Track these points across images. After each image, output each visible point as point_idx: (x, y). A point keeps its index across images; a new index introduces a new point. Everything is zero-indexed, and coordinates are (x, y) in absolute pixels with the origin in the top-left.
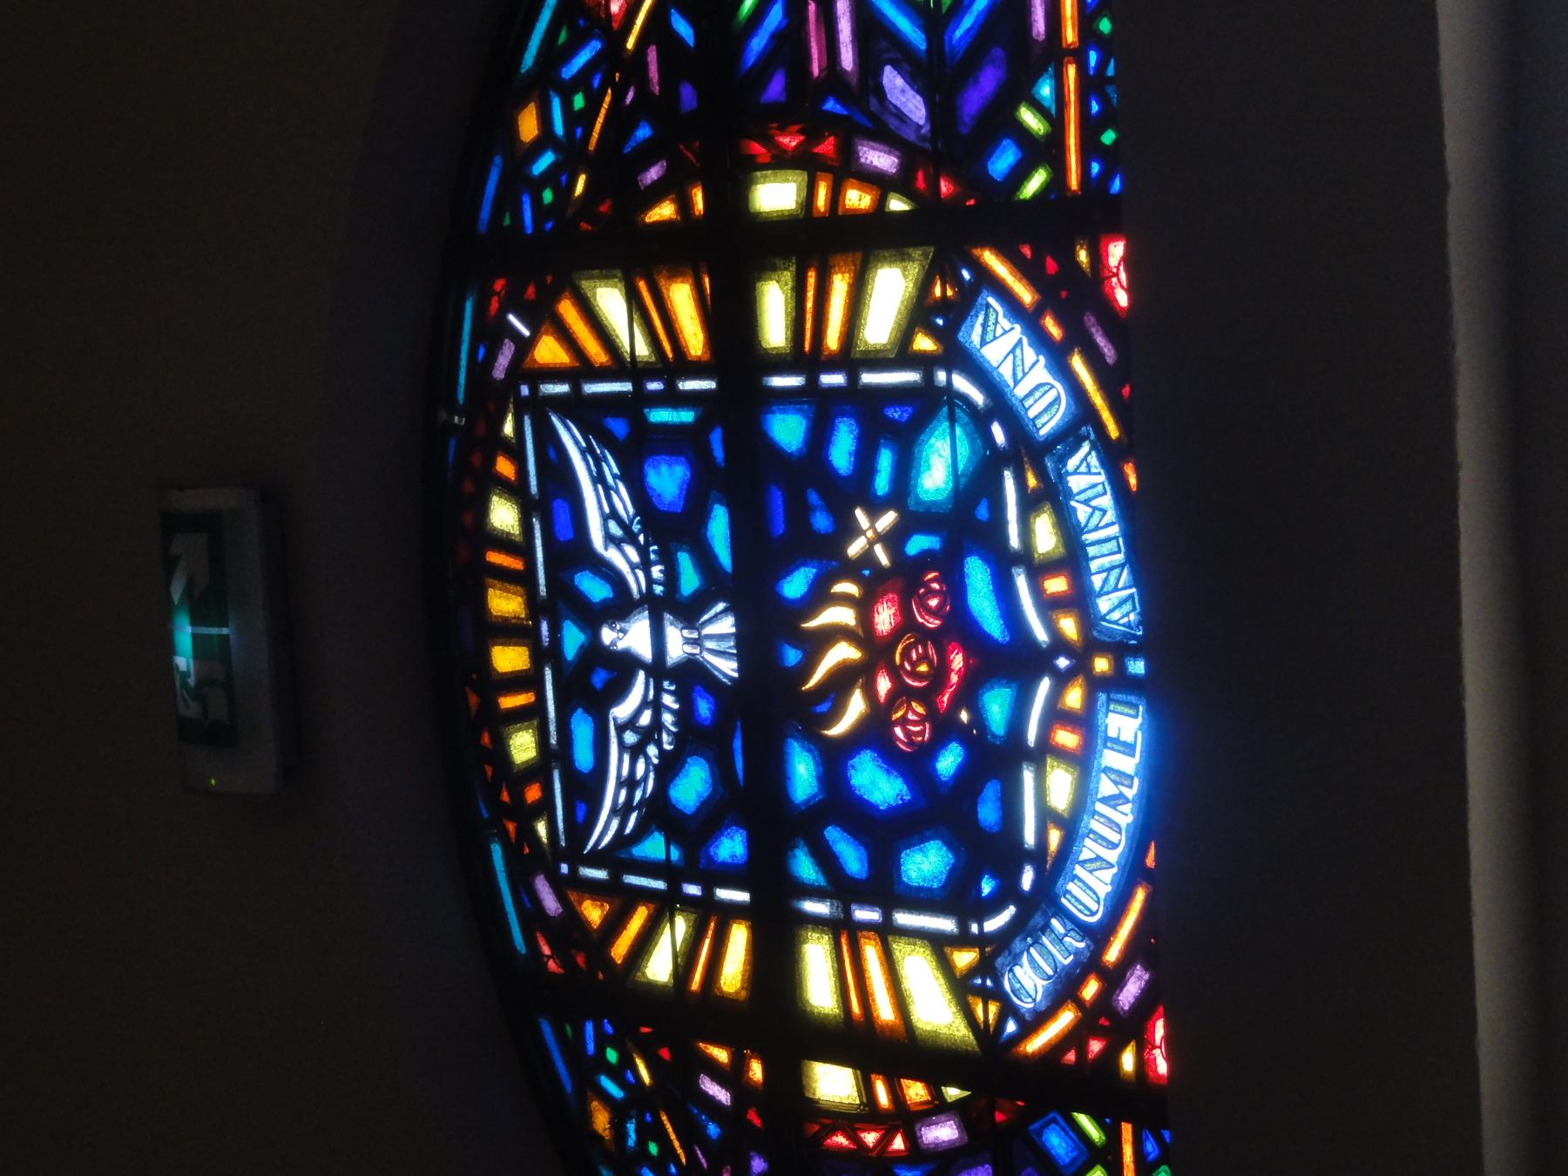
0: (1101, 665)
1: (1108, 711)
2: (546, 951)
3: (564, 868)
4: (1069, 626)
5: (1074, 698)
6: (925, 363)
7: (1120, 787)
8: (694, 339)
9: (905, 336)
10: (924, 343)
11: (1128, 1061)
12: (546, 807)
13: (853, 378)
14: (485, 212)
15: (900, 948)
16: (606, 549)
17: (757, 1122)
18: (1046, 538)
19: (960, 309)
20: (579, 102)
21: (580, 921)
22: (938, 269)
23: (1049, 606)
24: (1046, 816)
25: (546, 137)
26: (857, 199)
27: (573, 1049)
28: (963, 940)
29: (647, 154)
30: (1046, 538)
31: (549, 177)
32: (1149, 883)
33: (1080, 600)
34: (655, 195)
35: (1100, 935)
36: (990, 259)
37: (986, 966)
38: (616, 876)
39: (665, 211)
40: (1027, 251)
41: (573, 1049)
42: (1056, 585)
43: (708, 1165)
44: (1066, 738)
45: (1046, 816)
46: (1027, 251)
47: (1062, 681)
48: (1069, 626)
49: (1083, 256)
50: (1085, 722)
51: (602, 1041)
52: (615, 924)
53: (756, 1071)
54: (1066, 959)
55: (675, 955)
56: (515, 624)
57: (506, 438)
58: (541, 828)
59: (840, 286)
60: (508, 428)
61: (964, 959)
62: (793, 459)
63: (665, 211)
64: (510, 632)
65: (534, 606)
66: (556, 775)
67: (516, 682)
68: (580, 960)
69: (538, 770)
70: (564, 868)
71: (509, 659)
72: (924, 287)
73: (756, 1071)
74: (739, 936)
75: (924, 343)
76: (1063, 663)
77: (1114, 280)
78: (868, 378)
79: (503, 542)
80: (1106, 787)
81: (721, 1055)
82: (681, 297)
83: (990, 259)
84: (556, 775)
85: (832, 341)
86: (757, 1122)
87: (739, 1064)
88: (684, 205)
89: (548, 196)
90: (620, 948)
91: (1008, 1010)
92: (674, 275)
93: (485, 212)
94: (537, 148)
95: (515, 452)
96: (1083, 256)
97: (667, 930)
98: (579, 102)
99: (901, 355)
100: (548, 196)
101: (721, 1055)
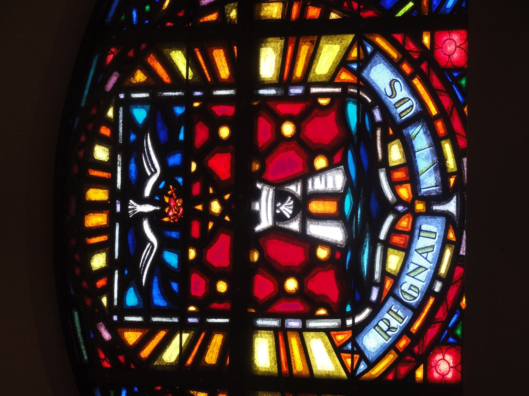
1: (419, 236)
3: (115, 318)
4: (404, 192)
5: (404, 223)
8: (224, 72)
10: (344, 76)
11: (419, 374)
12: (108, 290)
14: (111, 14)
15: (307, 336)
17: (391, 130)
21: (124, 342)
22: (358, 42)
28: (343, 328)
32: (440, 281)
36: (380, 41)
37: (353, 340)
38: (147, 319)
39: (213, 17)
47: (399, 216)
48: (404, 192)
54: (387, 341)
56: (96, 210)
58: (104, 300)
59: (304, 50)
60: (110, 113)
61: (340, 338)
63: (213, 17)
65: (114, 194)
67: (98, 231)
68: (122, 358)
70: (115, 318)
74: (218, 340)
75: (344, 76)
79: (100, 165)
83: (380, 41)
85: (299, 72)
86: (391, 130)
88: (223, 15)
91: (363, 357)
93: (111, 14)
97: (178, 336)
99: (331, 81)
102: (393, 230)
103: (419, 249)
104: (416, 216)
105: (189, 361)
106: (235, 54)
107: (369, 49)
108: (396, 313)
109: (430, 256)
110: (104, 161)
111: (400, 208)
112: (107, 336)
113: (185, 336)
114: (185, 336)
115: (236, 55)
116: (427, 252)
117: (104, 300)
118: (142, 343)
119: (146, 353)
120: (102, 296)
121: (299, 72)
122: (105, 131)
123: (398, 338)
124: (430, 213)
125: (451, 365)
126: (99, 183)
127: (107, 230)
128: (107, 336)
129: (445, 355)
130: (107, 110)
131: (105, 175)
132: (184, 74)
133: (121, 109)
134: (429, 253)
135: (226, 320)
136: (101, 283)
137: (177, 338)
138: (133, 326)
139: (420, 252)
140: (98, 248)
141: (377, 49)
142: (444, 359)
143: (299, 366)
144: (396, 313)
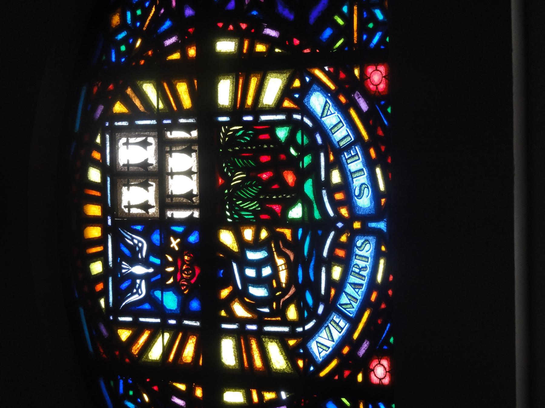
0: (357, 225)
2: (102, 351)
6: (289, 112)
7: (351, 301)
8: (187, 102)
9: (280, 101)
10: (287, 104)
11: (360, 378)
12: (104, 293)
13: (256, 118)
16: (190, 135)
18: (336, 177)
19: (305, 90)
20: (139, 12)
23: (336, 205)
24: (330, 281)
25: (123, 25)
26: (260, 48)
27: (113, 392)
29: (168, 34)
30: (336, 177)
31: (124, 41)
33: (349, 202)
34: (172, 49)
35: (354, 322)
36: (318, 73)
39: (176, 56)
40: (127, 360)
41: (113, 392)
42: (339, 196)
43: (279, 242)
44: (341, 253)
45: (330, 281)
46: (127, 360)
48: (344, 212)
49: (357, 72)
50: (349, 247)
51: (127, 388)
52: (133, 339)
53: (199, 393)
55: (164, 347)
57: (97, 144)
59: (254, 82)
60: (98, 140)
61: (292, 342)
62: (320, 38)
63: (176, 56)
64: (94, 221)
66: (110, 279)
67: (95, 242)
69: (102, 278)
71: (94, 232)
72: (290, 81)
73: (199, 393)
75: (287, 104)
76: (340, 225)
77: (369, 79)
78: (264, 118)
80: (352, 279)
81: (182, 387)
82: (182, 88)
83: (318, 73)
84: (110, 279)
85: (249, 101)
87: (191, 390)
88: (184, 54)
89: (123, 48)
90: (136, 349)
92: (181, 79)
94: (119, 30)
95: (101, 149)
96: (357, 72)
97: (161, 337)
98: (139, 12)
99: (277, 108)
100: (123, 48)
101: (182, 387)
102: (336, 244)
103: (320, 343)
104: (354, 234)
105: (172, 357)
106: (195, 86)
107: (308, 79)
108: (338, 324)
109: (324, 354)
110: (93, 167)
111: (340, 225)
112: (104, 331)
113: (167, 336)
114: (167, 336)
115: (196, 87)
116: (324, 350)
117: (102, 302)
118: (133, 339)
119: (136, 349)
120: (100, 297)
121: (249, 101)
122: (97, 155)
123: (367, 295)
124: (365, 231)
125: (387, 369)
126: (94, 201)
127: (102, 241)
128: (104, 331)
129: (380, 361)
130: (95, 138)
131: (98, 194)
132: (155, 104)
133: (108, 136)
134: (324, 351)
135: (198, 324)
136: (100, 287)
137: (160, 339)
138: (125, 325)
139: (319, 345)
140: (95, 257)
141: (316, 80)
142: (379, 363)
143: (258, 363)
144: (338, 324)
